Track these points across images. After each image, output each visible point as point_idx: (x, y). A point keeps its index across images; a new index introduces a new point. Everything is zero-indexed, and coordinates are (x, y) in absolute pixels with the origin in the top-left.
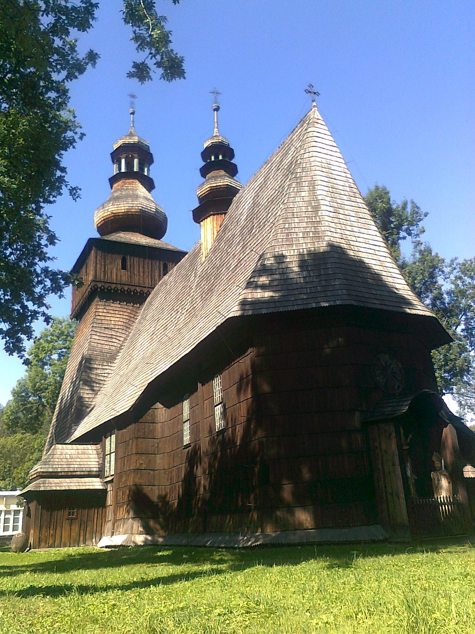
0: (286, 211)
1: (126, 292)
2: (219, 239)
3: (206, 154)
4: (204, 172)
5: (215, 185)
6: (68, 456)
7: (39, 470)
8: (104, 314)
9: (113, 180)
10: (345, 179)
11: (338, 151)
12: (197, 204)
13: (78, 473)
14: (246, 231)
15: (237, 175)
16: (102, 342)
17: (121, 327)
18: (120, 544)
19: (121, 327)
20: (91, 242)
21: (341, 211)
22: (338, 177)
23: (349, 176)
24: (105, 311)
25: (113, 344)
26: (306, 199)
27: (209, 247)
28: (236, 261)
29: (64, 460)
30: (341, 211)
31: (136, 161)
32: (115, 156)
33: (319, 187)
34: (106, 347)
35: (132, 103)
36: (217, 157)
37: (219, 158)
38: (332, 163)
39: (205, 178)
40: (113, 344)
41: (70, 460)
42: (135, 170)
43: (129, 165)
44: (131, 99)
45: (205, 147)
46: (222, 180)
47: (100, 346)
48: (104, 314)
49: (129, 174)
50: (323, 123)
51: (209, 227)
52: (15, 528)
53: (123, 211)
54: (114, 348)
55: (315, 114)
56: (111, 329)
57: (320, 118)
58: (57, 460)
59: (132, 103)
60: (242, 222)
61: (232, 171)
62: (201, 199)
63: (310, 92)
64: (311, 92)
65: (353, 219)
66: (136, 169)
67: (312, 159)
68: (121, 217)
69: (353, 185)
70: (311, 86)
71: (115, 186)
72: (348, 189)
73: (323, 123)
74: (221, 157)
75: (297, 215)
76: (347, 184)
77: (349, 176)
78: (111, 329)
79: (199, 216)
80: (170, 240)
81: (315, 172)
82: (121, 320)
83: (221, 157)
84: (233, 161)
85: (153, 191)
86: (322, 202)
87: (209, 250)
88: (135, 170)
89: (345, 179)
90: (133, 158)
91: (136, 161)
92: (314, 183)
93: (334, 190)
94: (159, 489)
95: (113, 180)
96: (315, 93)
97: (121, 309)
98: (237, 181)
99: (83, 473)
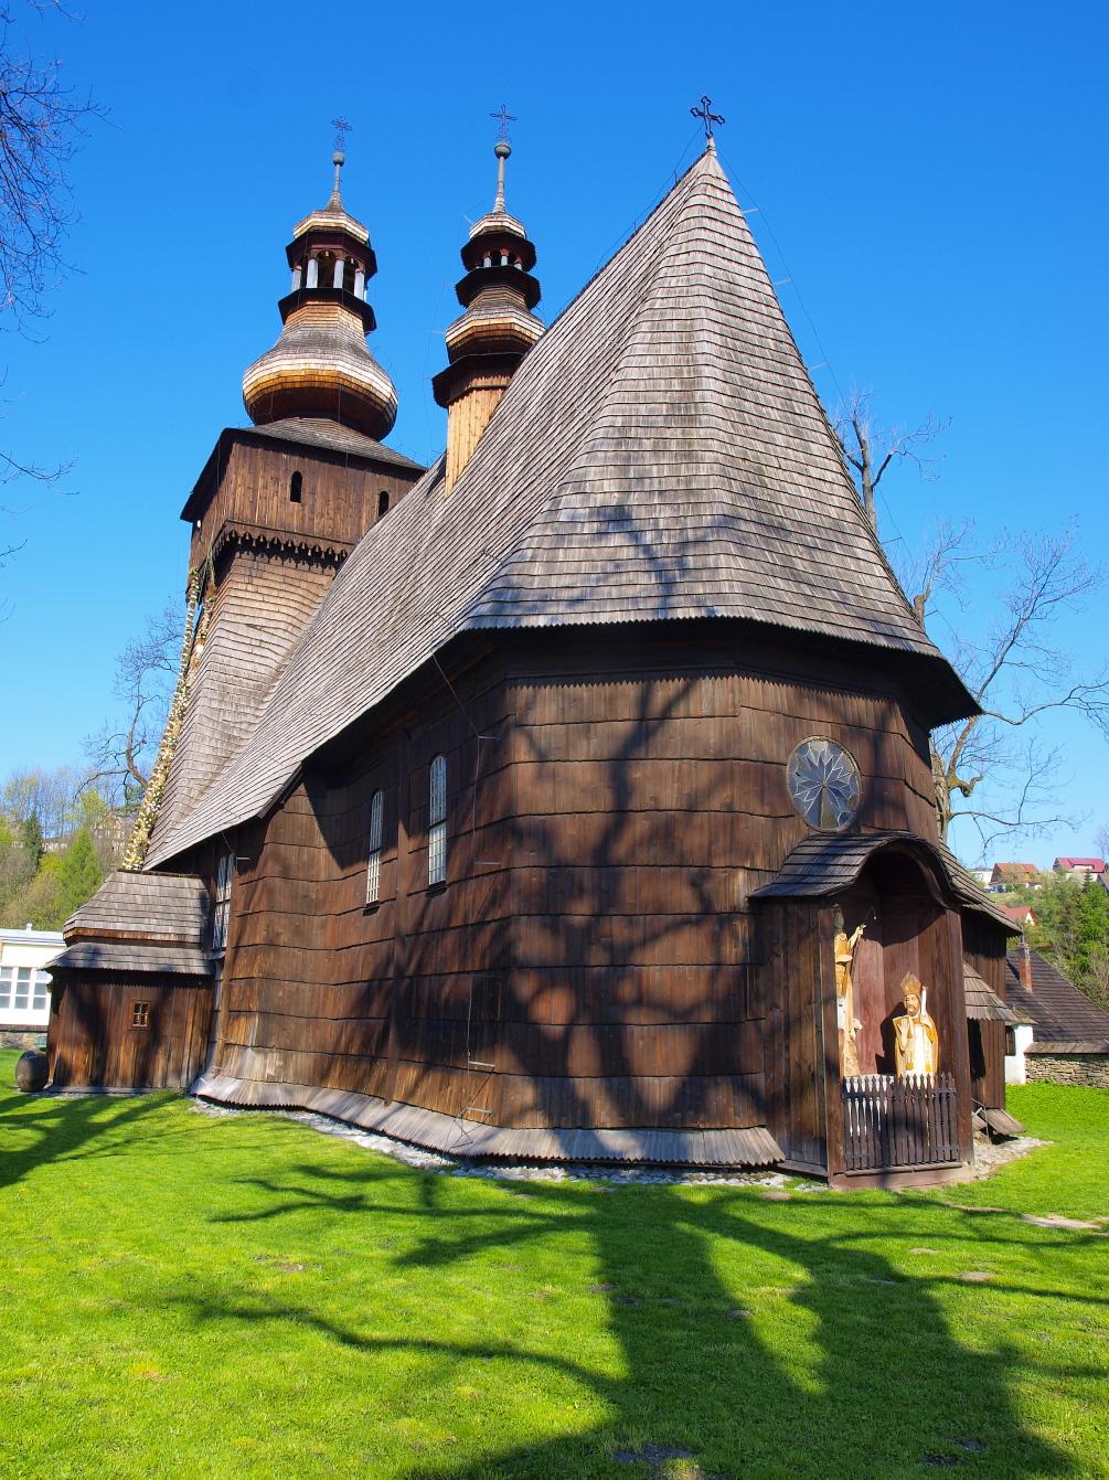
0: (620, 386)
1: (323, 556)
2: (484, 442)
3: (472, 252)
4: (467, 292)
5: (486, 323)
6: (139, 899)
7: (76, 925)
8: (248, 595)
9: (289, 305)
10: (767, 321)
11: (756, 253)
12: (443, 363)
13: (158, 937)
14: (536, 428)
15: (540, 305)
16: (239, 655)
17: (282, 626)
18: (224, 1100)
19: (282, 626)
20: (230, 437)
21: (748, 394)
22: (749, 315)
23: (776, 313)
24: (250, 588)
25: (262, 661)
26: (670, 360)
27: (463, 461)
28: (507, 497)
29: (130, 907)
30: (748, 394)
31: (339, 266)
32: (297, 253)
33: (704, 336)
34: (249, 666)
35: (340, 140)
36: (496, 260)
37: (500, 263)
38: (740, 280)
39: (467, 306)
40: (262, 661)
41: (143, 908)
42: (335, 286)
43: (325, 274)
44: (337, 132)
45: (474, 232)
46: (499, 314)
47: (234, 662)
48: (248, 595)
49: (325, 293)
50: (725, 186)
51: (469, 416)
52: (143, 1022)
53: (303, 374)
54: (262, 669)
55: (710, 166)
56: (260, 628)
57: (721, 174)
58: (116, 905)
59: (340, 140)
60: (533, 410)
61: (531, 294)
62: (453, 351)
63: (701, 114)
64: (707, 116)
65: (775, 414)
66: (338, 283)
67: (693, 269)
68: (297, 385)
69: (782, 336)
70: (706, 101)
71: (291, 318)
72: (772, 344)
73: (725, 186)
74: (504, 261)
75: (645, 398)
76: (771, 333)
77: (776, 313)
78: (260, 628)
79: (448, 389)
80: (396, 445)
81: (696, 298)
82: (284, 610)
83: (504, 261)
84: (532, 273)
85: (373, 334)
86: (707, 371)
87: (461, 468)
88: (335, 286)
89: (767, 321)
90: (333, 258)
91: (339, 266)
92: (692, 326)
93: (738, 343)
94: (313, 991)
95: (289, 305)
96: (714, 118)
97: (284, 587)
98: (535, 317)
99: (167, 938)
